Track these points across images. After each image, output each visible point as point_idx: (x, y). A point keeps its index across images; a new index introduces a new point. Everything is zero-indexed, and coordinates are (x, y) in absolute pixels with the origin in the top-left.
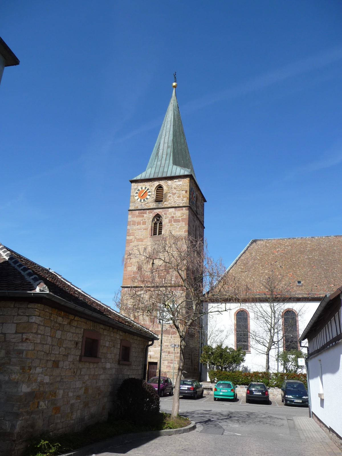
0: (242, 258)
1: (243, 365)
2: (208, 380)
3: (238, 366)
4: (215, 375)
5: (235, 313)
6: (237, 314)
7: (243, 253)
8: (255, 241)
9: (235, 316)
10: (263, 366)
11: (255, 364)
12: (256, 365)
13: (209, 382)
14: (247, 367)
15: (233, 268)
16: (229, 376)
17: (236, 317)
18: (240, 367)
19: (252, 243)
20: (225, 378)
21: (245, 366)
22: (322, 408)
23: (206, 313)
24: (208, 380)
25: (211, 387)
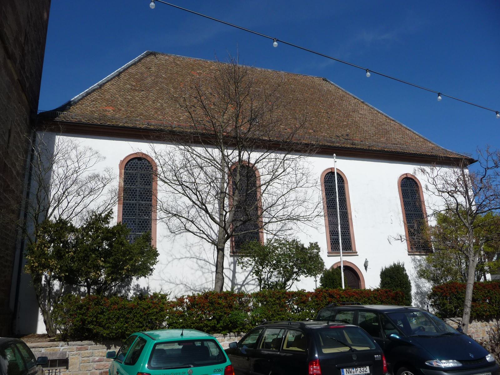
0: (130, 70)
1: (138, 286)
2: (41, 329)
3: (124, 287)
4: (83, 311)
5: (122, 162)
6: (126, 164)
7: (132, 65)
8: (154, 54)
9: (120, 169)
10: (186, 285)
11: (167, 282)
12: (171, 283)
13: (43, 336)
14: (148, 288)
15: (112, 82)
16: (130, 312)
17: (123, 171)
18: (129, 290)
19: (148, 55)
20: (118, 318)
21: (142, 287)
22: (368, 260)
23: (157, 193)
24: (41, 329)
25: (64, 354)
